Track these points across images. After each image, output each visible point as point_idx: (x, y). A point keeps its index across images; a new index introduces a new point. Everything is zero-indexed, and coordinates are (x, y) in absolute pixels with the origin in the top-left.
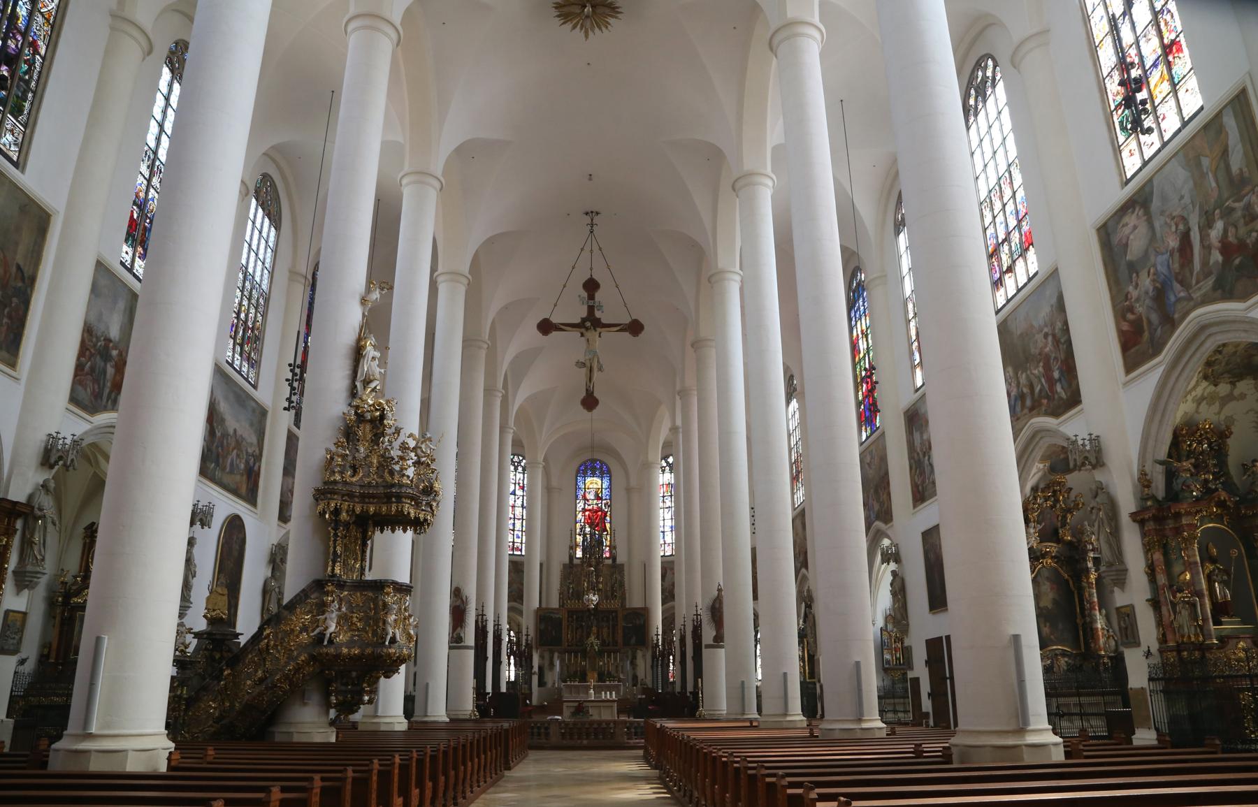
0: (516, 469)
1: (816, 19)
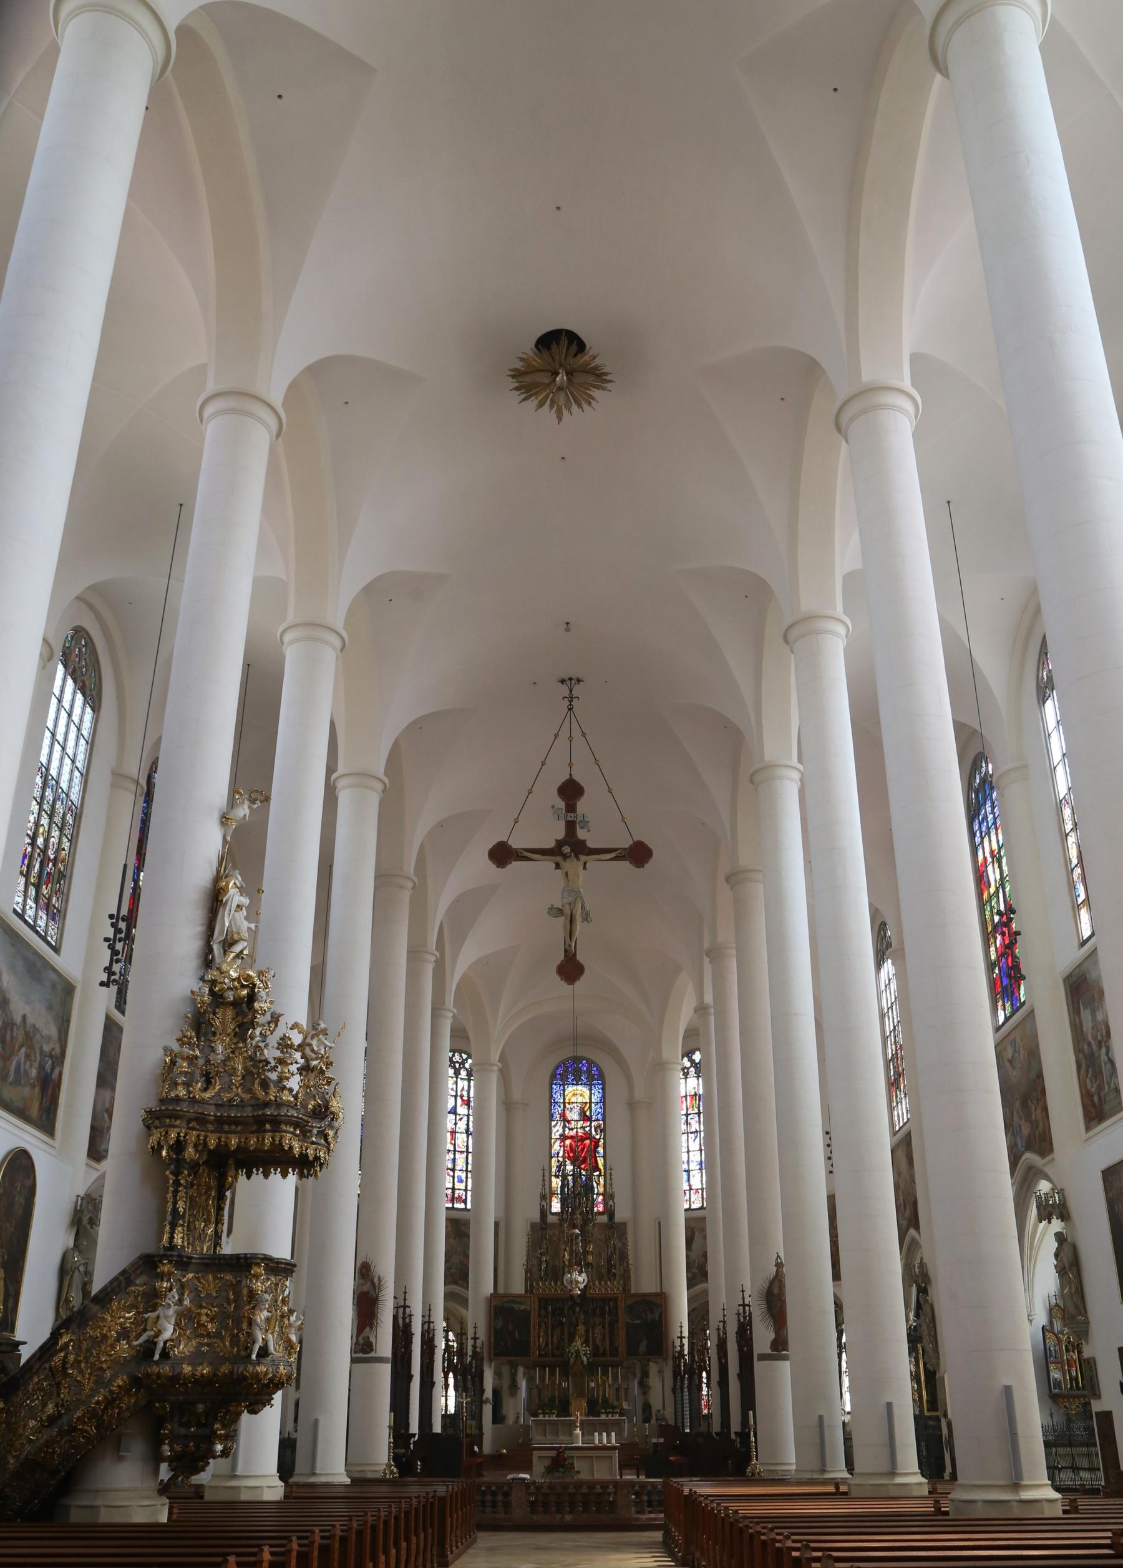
1: (906, 383)
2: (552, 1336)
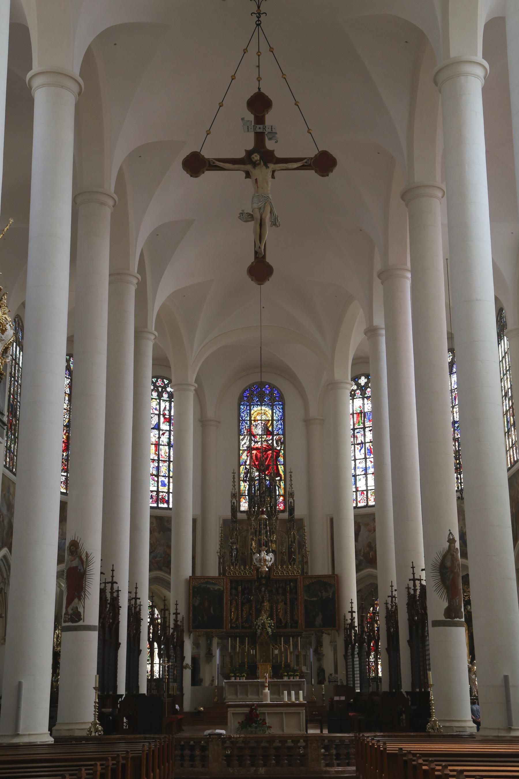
0: (160, 396)
1: (479, 57)
2: (242, 611)
